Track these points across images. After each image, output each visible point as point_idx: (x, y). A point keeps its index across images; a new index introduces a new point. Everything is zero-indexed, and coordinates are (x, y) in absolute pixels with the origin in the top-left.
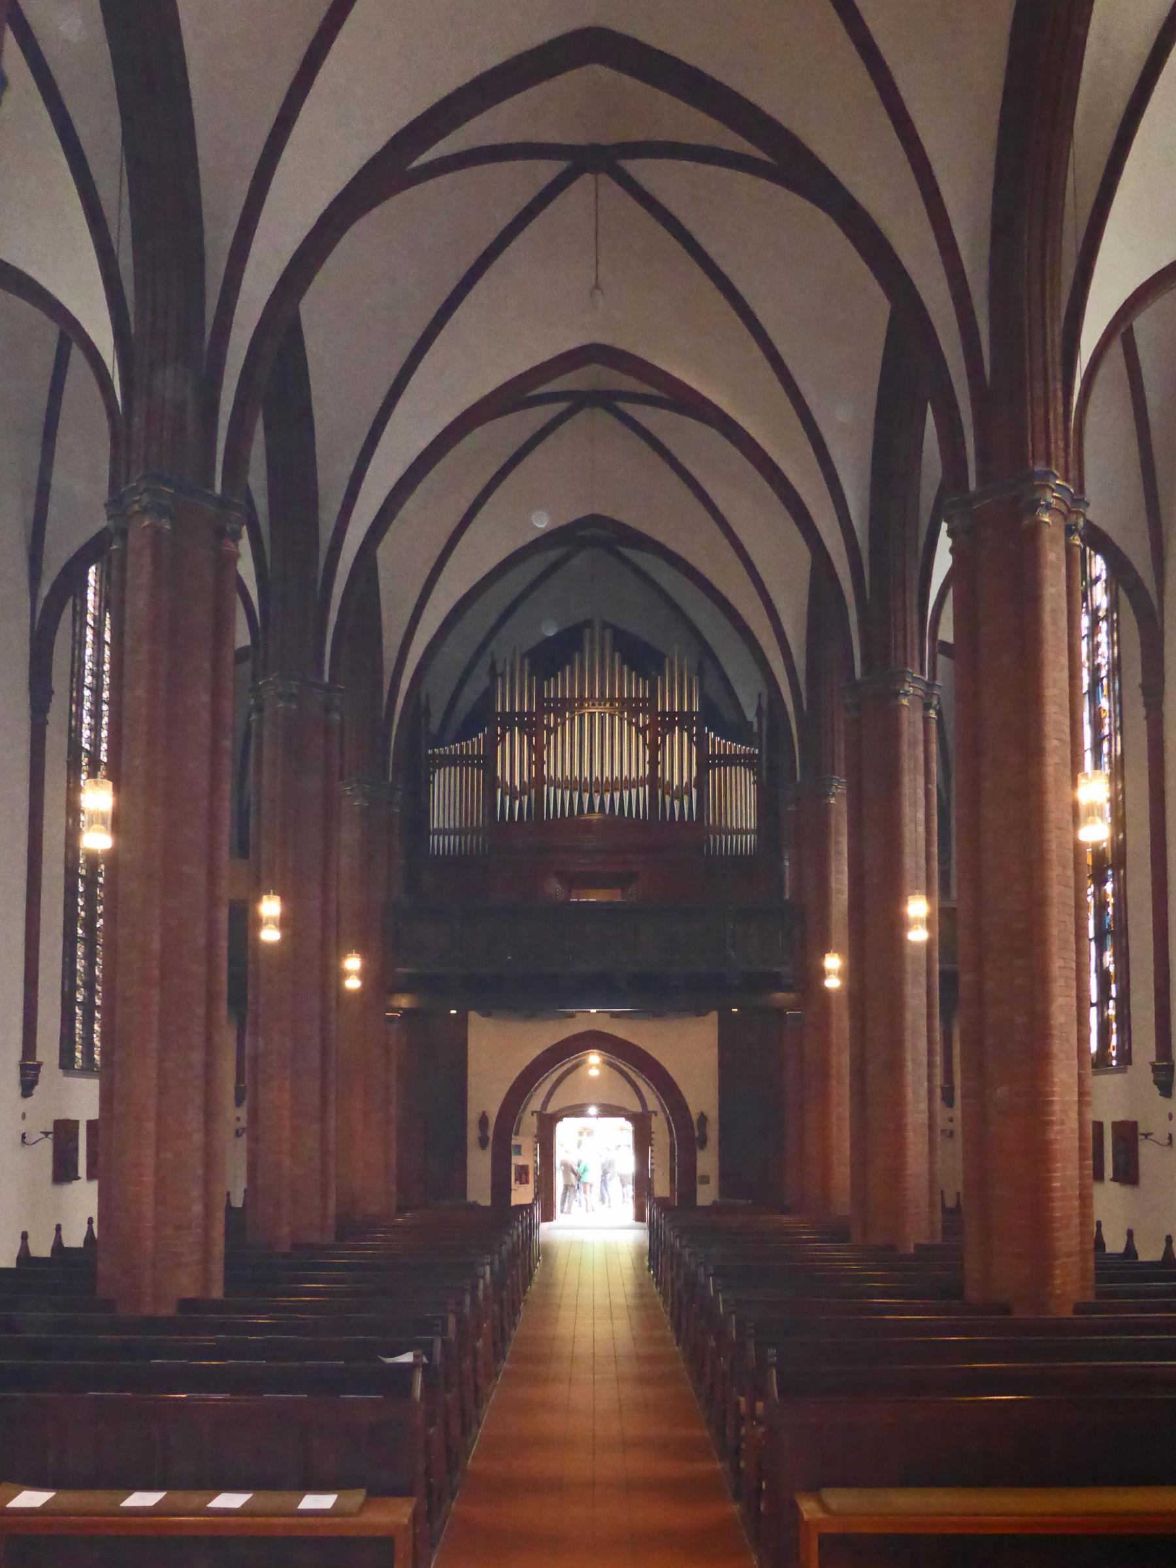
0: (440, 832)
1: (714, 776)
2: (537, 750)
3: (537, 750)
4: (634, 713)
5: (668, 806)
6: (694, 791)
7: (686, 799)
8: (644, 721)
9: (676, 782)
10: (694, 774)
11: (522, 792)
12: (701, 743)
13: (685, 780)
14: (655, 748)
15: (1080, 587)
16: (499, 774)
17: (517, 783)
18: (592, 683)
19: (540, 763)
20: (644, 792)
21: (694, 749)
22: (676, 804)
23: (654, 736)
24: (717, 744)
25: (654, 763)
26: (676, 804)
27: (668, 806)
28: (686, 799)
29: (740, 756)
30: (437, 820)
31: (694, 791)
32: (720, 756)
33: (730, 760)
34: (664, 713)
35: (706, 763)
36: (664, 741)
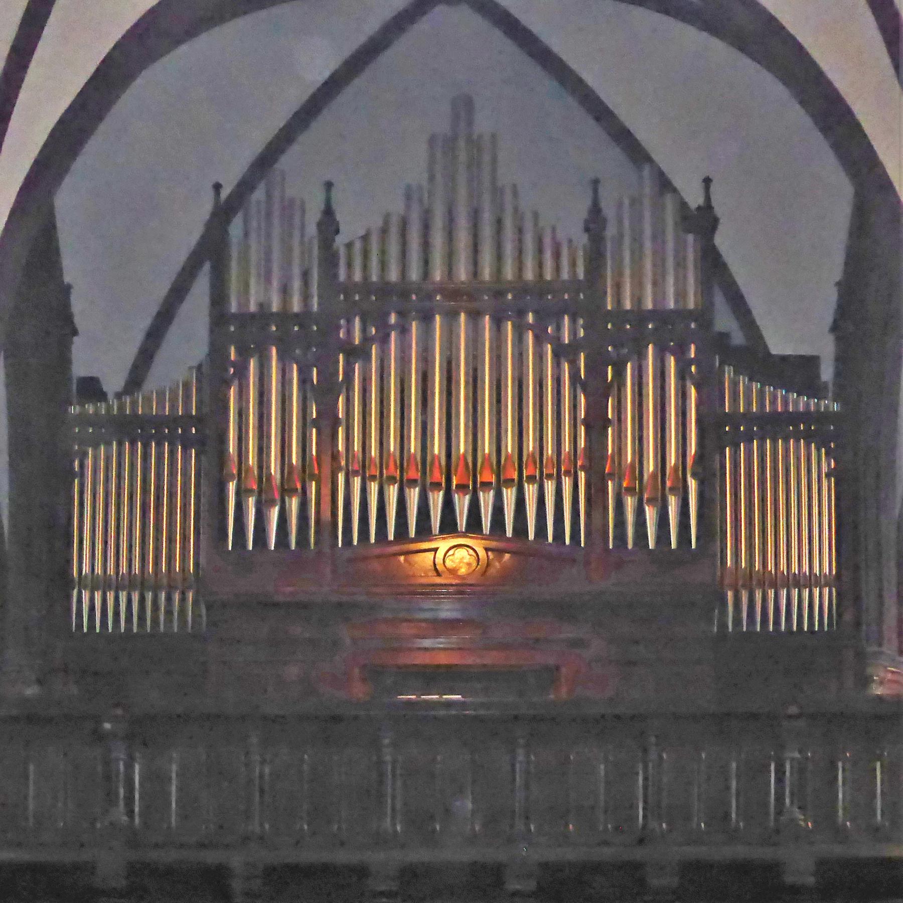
0: (104, 584)
1: (740, 460)
2: (325, 392)
3: (325, 392)
4: (549, 315)
5: (630, 517)
6: (692, 484)
7: (673, 503)
8: (573, 332)
9: (650, 466)
10: (692, 448)
11: (286, 491)
12: (709, 384)
13: (672, 458)
14: (598, 390)
15: (847, 576)
16: (232, 448)
17: (274, 468)
18: (92, 608)
19: (328, 423)
20: (572, 489)
21: (693, 392)
22: (650, 514)
23: (596, 368)
24: (744, 394)
25: (596, 424)
26: (650, 514)
27: (630, 517)
28: (673, 503)
29: (795, 418)
30: (87, 560)
31: (692, 484)
32: (748, 417)
33: (774, 425)
34: (619, 315)
35: (717, 431)
36: (620, 374)
